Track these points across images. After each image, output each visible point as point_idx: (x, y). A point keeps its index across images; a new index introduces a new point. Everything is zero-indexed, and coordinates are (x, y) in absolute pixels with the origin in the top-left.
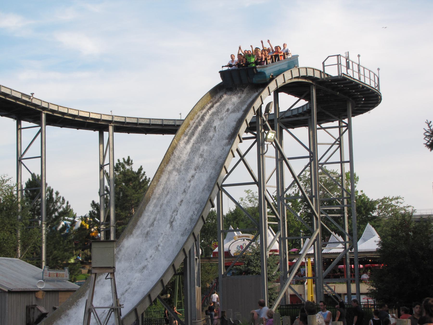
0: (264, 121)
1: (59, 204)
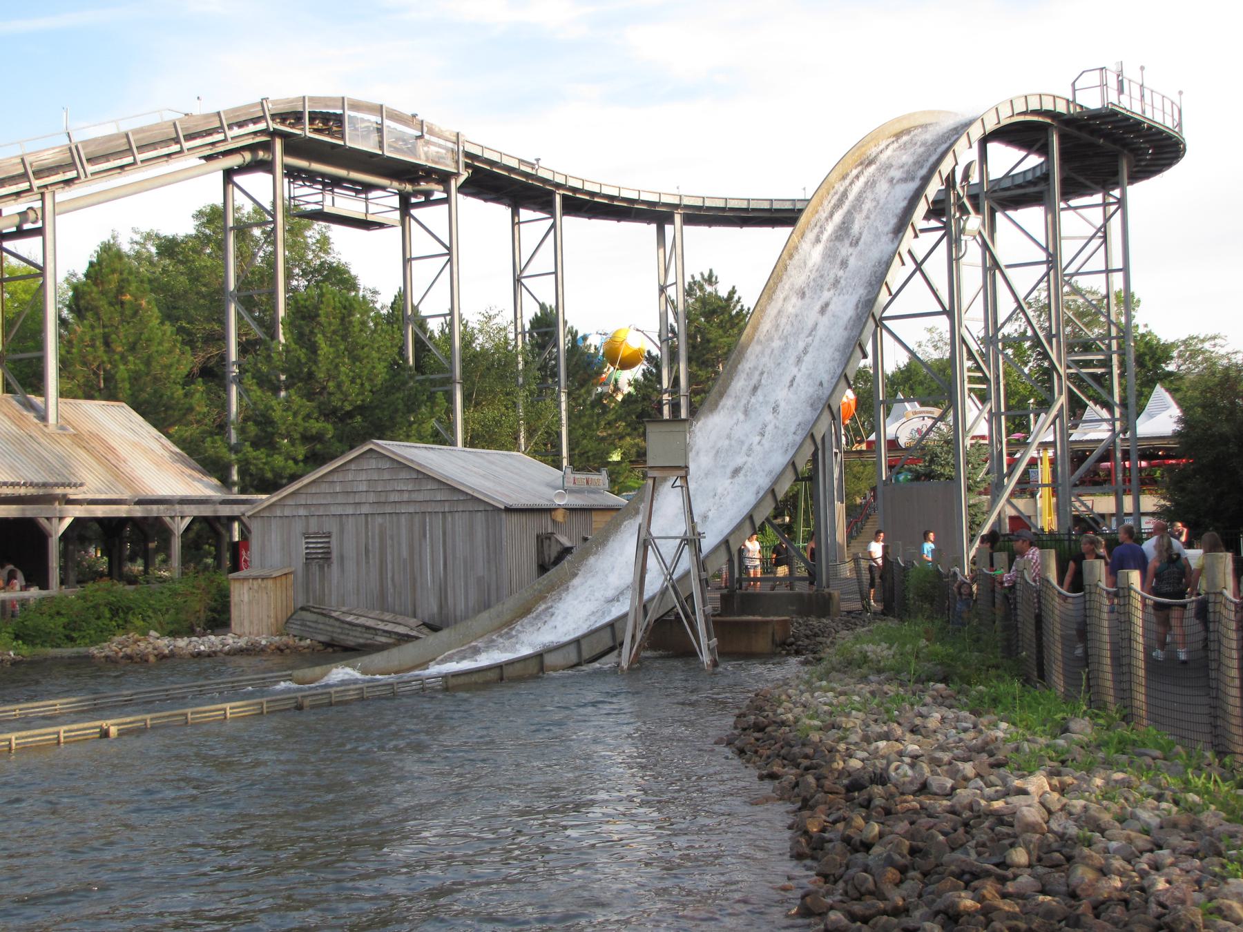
0: (959, 198)
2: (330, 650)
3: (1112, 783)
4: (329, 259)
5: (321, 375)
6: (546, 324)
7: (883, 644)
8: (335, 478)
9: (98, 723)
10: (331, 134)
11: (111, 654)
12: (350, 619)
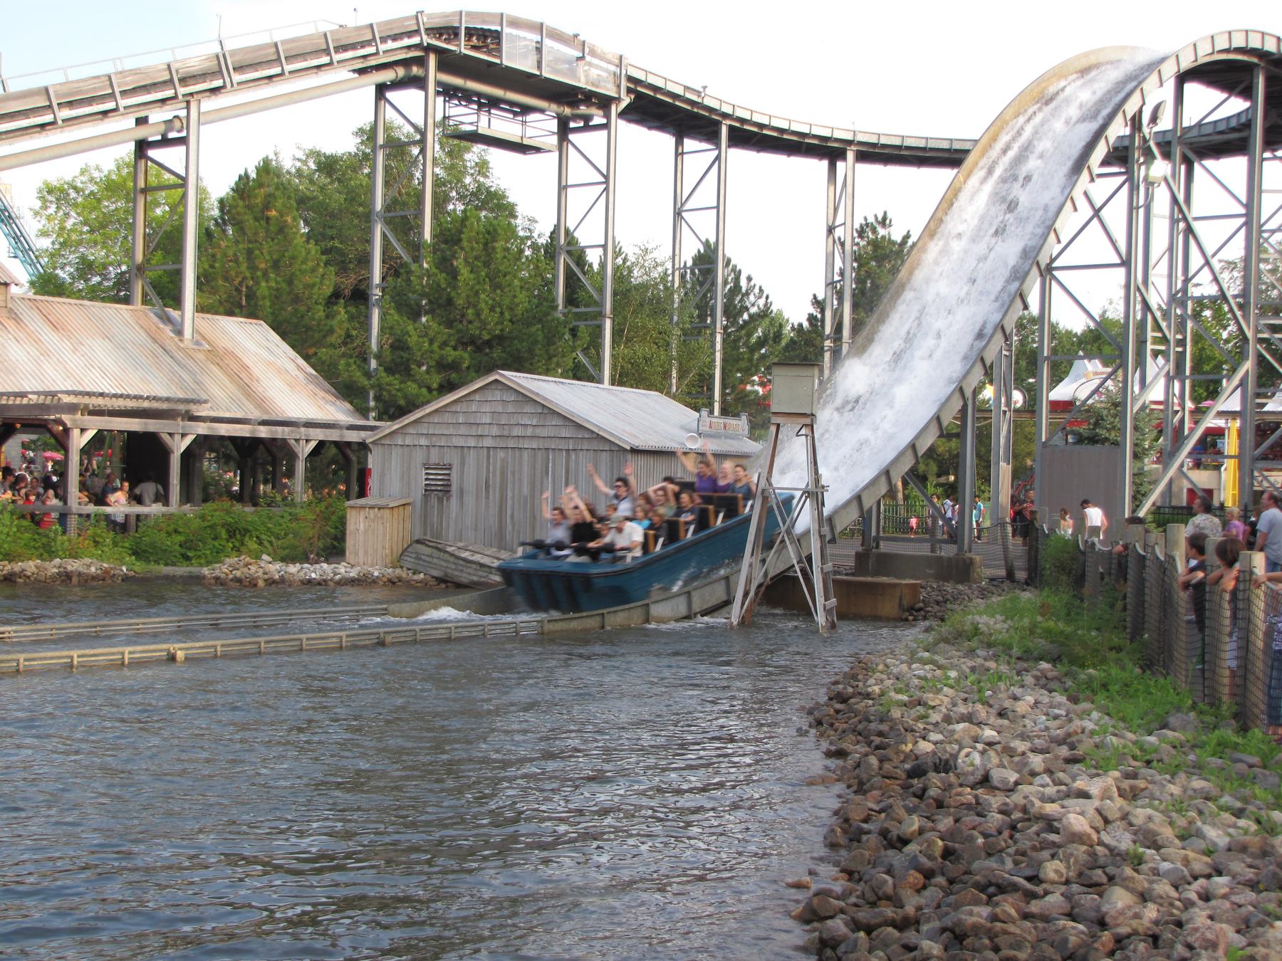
0: (1145, 140)
1: (752, 298)
2: (443, 586)
3: (1190, 792)
4: (488, 182)
5: (460, 302)
6: (707, 260)
7: (998, 617)
8: (458, 408)
9: (165, 646)
10: (489, 53)
11: (223, 576)
12: (465, 555)
